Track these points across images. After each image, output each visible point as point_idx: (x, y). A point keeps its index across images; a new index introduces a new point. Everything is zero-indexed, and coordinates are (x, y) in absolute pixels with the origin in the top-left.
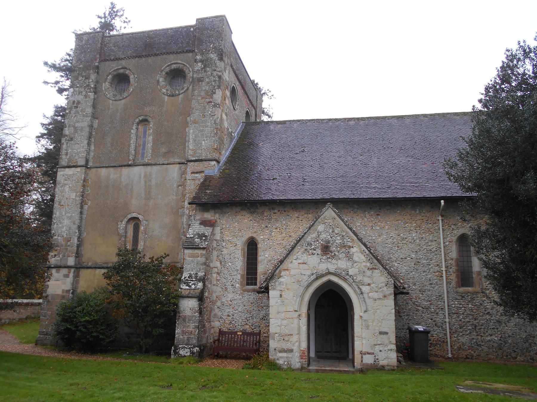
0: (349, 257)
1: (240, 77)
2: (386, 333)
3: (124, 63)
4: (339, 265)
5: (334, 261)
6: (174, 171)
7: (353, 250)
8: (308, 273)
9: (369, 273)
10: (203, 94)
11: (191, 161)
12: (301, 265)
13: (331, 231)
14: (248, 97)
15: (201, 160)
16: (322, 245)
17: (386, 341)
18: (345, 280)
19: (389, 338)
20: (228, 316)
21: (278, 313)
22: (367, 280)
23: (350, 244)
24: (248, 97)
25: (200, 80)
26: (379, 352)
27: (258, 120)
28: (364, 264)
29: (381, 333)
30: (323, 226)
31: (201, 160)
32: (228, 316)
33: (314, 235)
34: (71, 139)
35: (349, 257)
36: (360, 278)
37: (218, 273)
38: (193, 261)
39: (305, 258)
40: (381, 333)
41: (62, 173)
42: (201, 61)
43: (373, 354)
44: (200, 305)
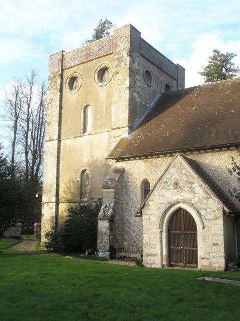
0: (192, 190)
1: (154, 62)
2: (217, 244)
3: (74, 69)
4: (185, 197)
5: (181, 194)
6: (105, 135)
7: (194, 185)
8: (166, 202)
9: (205, 201)
10: (119, 82)
11: (114, 129)
12: (161, 197)
13: (179, 172)
14: (166, 73)
15: (120, 128)
16: (174, 182)
17: (218, 251)
18: (171, 207)
19: (219, 249)
20: (134, 232)
21: (148, 229)
22: (204, 207)
23: (192, 181)
24: (166, 73)
25: (117, 72)
26: (213, 258)
27: (180, 89)
28: (202, 195)
29: (214, 244)
30: (175, 169)
31: (120, 128)
32: (134, 232)
33: (168, 176)
34: (50, 123)
35: (192, 190)
36: (199, 205)
37: (127, 204)
38: (107, 197)
39: (164, 192)
40: (214, 244)
41: (46, 145)
42: (118, 59)
43: (209, 259)
44: (110, 226)
